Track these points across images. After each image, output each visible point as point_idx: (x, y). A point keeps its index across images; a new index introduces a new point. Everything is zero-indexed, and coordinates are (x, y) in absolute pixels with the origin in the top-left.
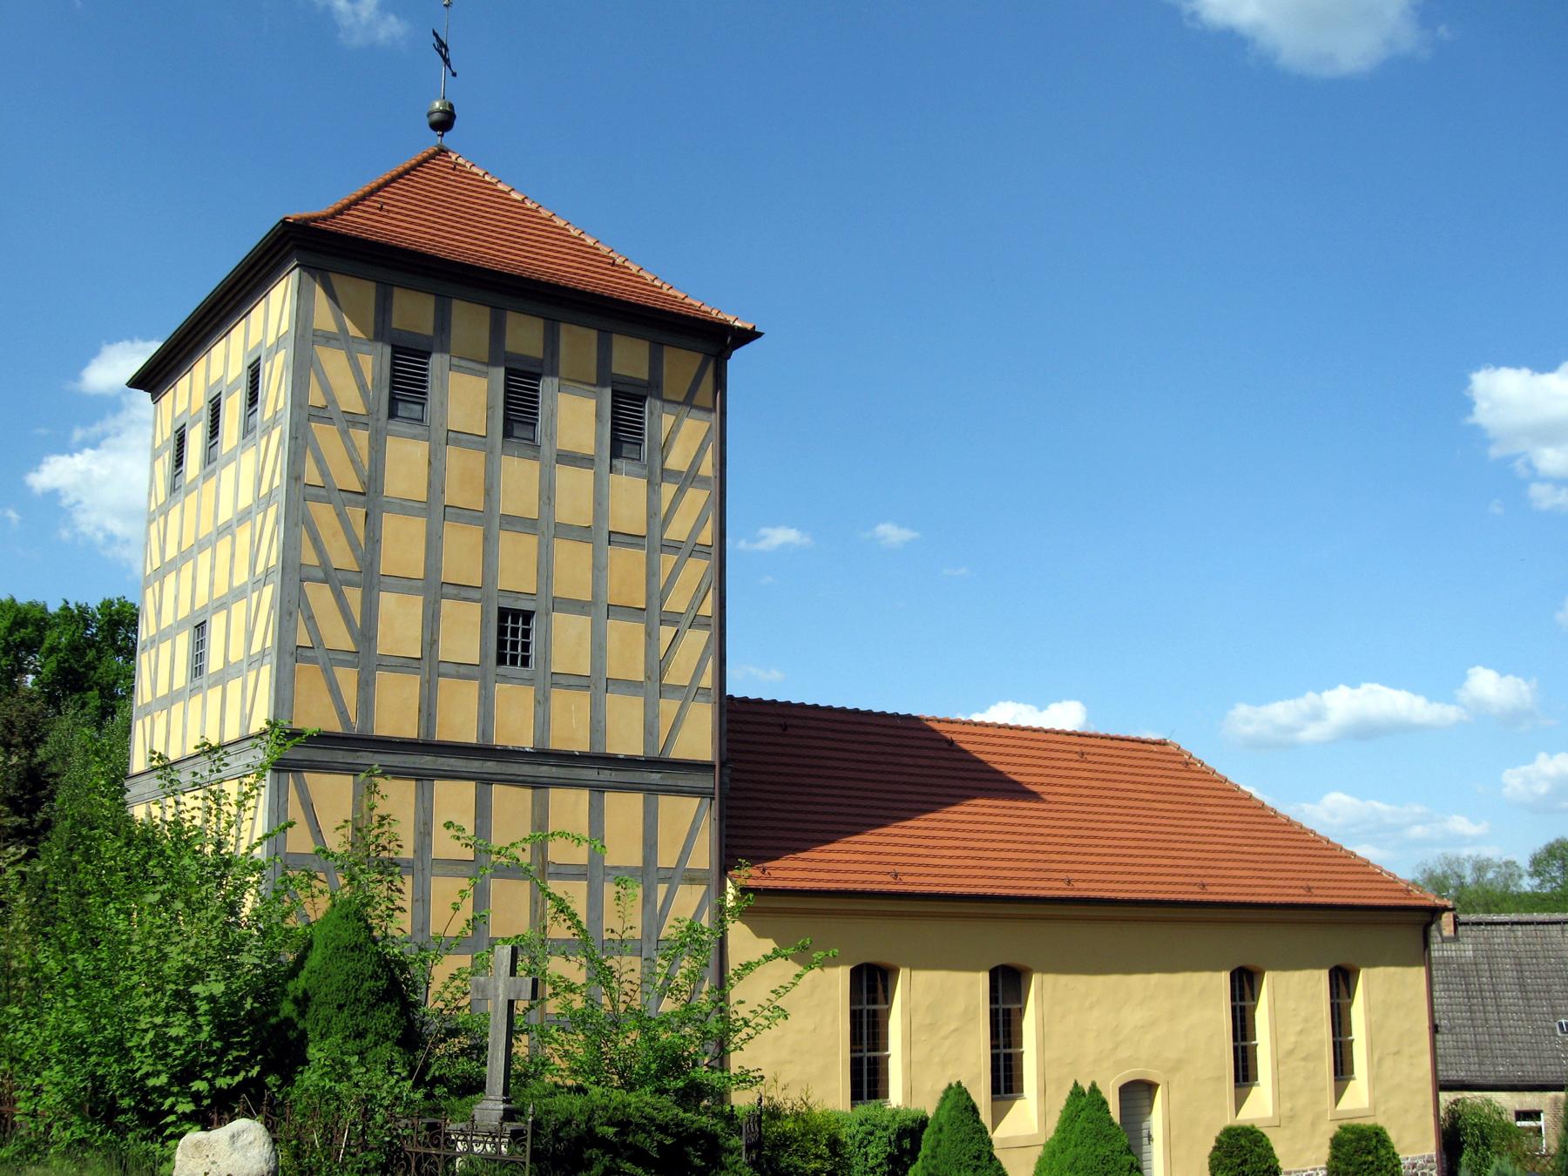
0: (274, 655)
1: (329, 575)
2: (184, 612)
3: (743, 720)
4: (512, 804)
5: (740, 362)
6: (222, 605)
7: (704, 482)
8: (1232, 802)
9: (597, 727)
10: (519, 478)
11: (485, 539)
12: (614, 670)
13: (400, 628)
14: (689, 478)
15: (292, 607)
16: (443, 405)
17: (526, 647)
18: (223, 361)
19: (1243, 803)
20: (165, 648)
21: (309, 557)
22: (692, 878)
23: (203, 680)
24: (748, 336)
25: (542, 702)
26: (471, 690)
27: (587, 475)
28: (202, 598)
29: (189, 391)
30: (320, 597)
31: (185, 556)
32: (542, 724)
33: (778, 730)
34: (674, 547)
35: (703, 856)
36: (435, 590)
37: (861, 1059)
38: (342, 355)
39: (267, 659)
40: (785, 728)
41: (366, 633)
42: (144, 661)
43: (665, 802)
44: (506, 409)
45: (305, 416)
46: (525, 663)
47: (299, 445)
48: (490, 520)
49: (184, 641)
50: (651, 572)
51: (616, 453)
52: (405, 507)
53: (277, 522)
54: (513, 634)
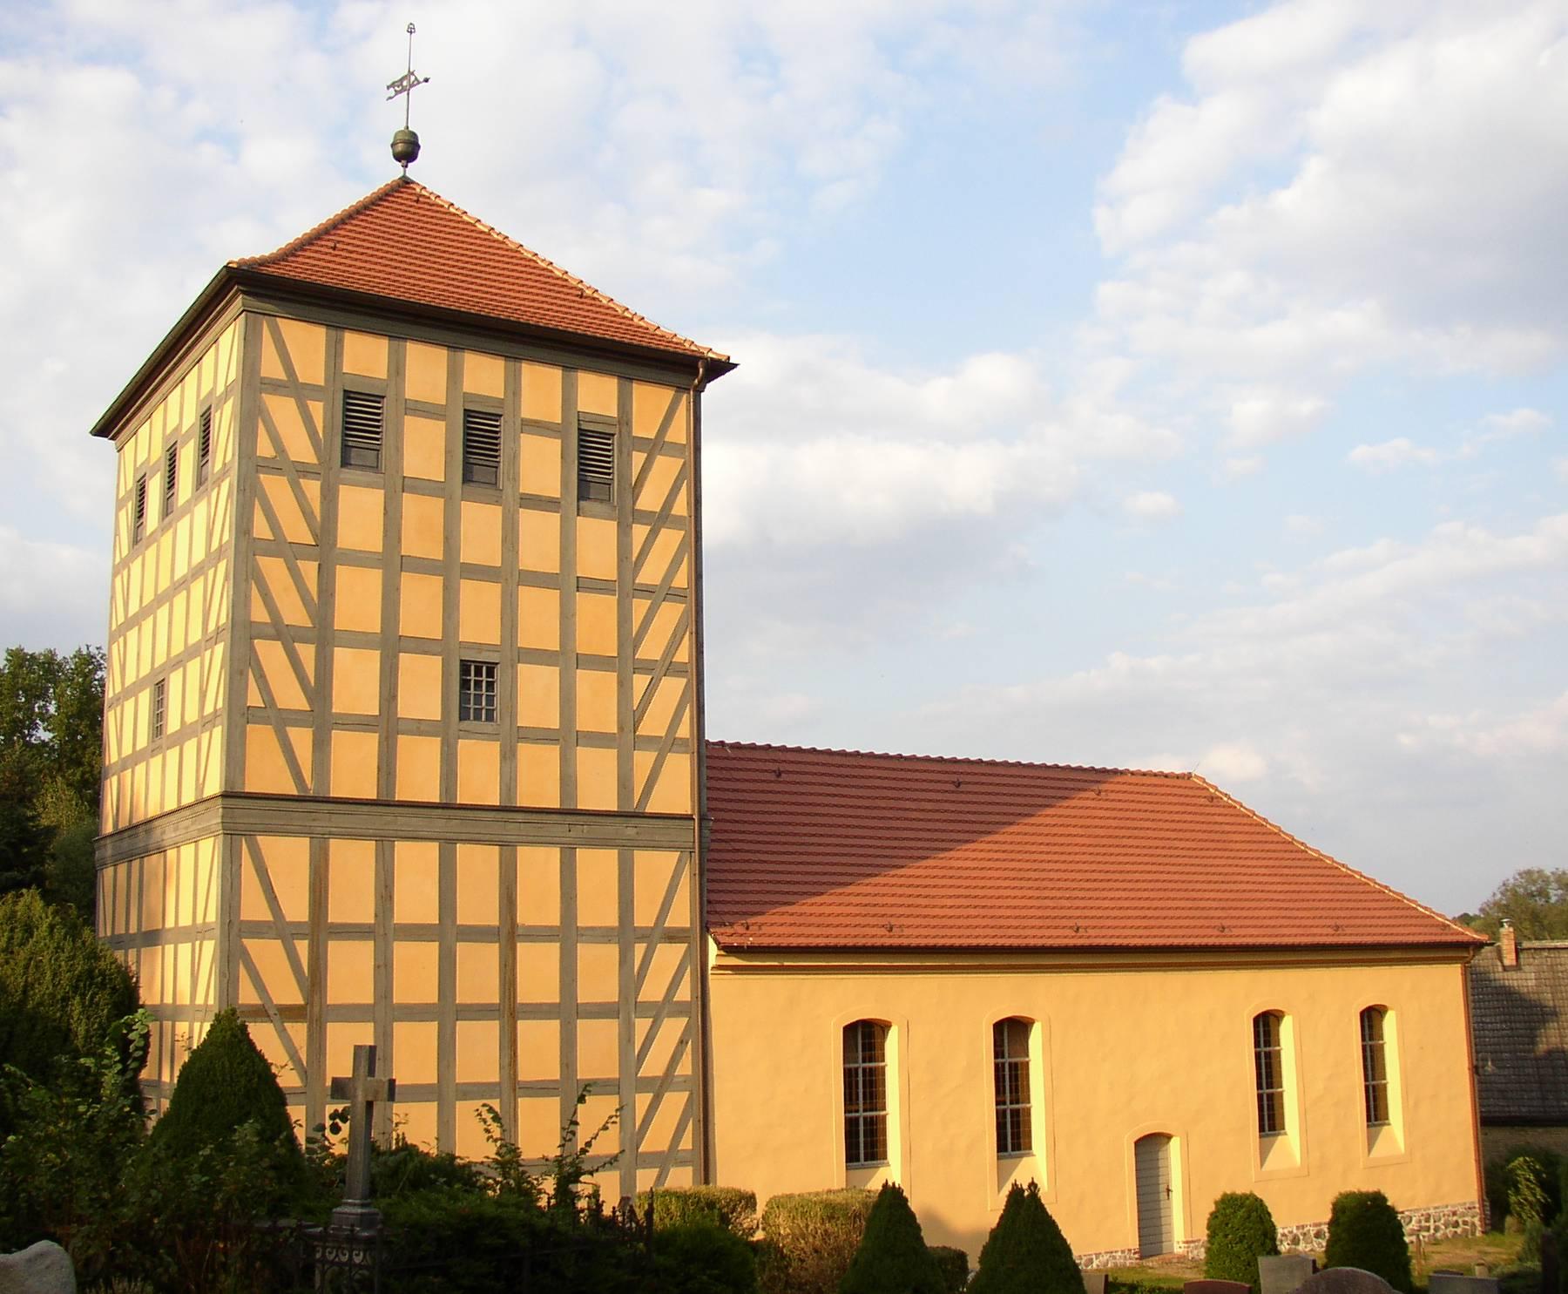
0: (225, 716)
1: (280, 632)
2: (145, 670)
3: (722, 767)
4: (478, 864)
5: (714, 391)
6: (178, 663)
7: (677, 522)
8: (1259, 838)
9: (568, 782)
10: (480, 526)
11: (446, 588)
12: (584, 723)
13: (356, 682)
14: (661, 519)
15: (242, 665)
16: (399, 450)
17: (490, 700)
18: (175, 409)
19: (1270, 838)
20: (129, 705)
21: (259, 614)
22: (672, 936)
23: (162, 741)
24: (720, 367)
25: (509, 756)
26: (433, 746)
27: (554, 518)
28: (161, 659)
29: (148, 438)
30: (271, 654)
31: (147, 611)
32: (509, 783)
33: (772, 777)
34: (647, 591)
35: (682, 914)
36: (391, 645)
37: (857, 1119)
38: (291, 403)
39: (218, 720)
40: (779, 775)
41: (319, 691)
42: (110, 719)
43: (642, 858)
44: (466, 453)
45: (251, 468)
46: (490, 718)
47: (248, 495)
48: (451, 570)
49: (145, 697)
50: (625, 958)
51: (582, 495)
52: (358, 559)
53: (226, 578)
54: (477, 685)
